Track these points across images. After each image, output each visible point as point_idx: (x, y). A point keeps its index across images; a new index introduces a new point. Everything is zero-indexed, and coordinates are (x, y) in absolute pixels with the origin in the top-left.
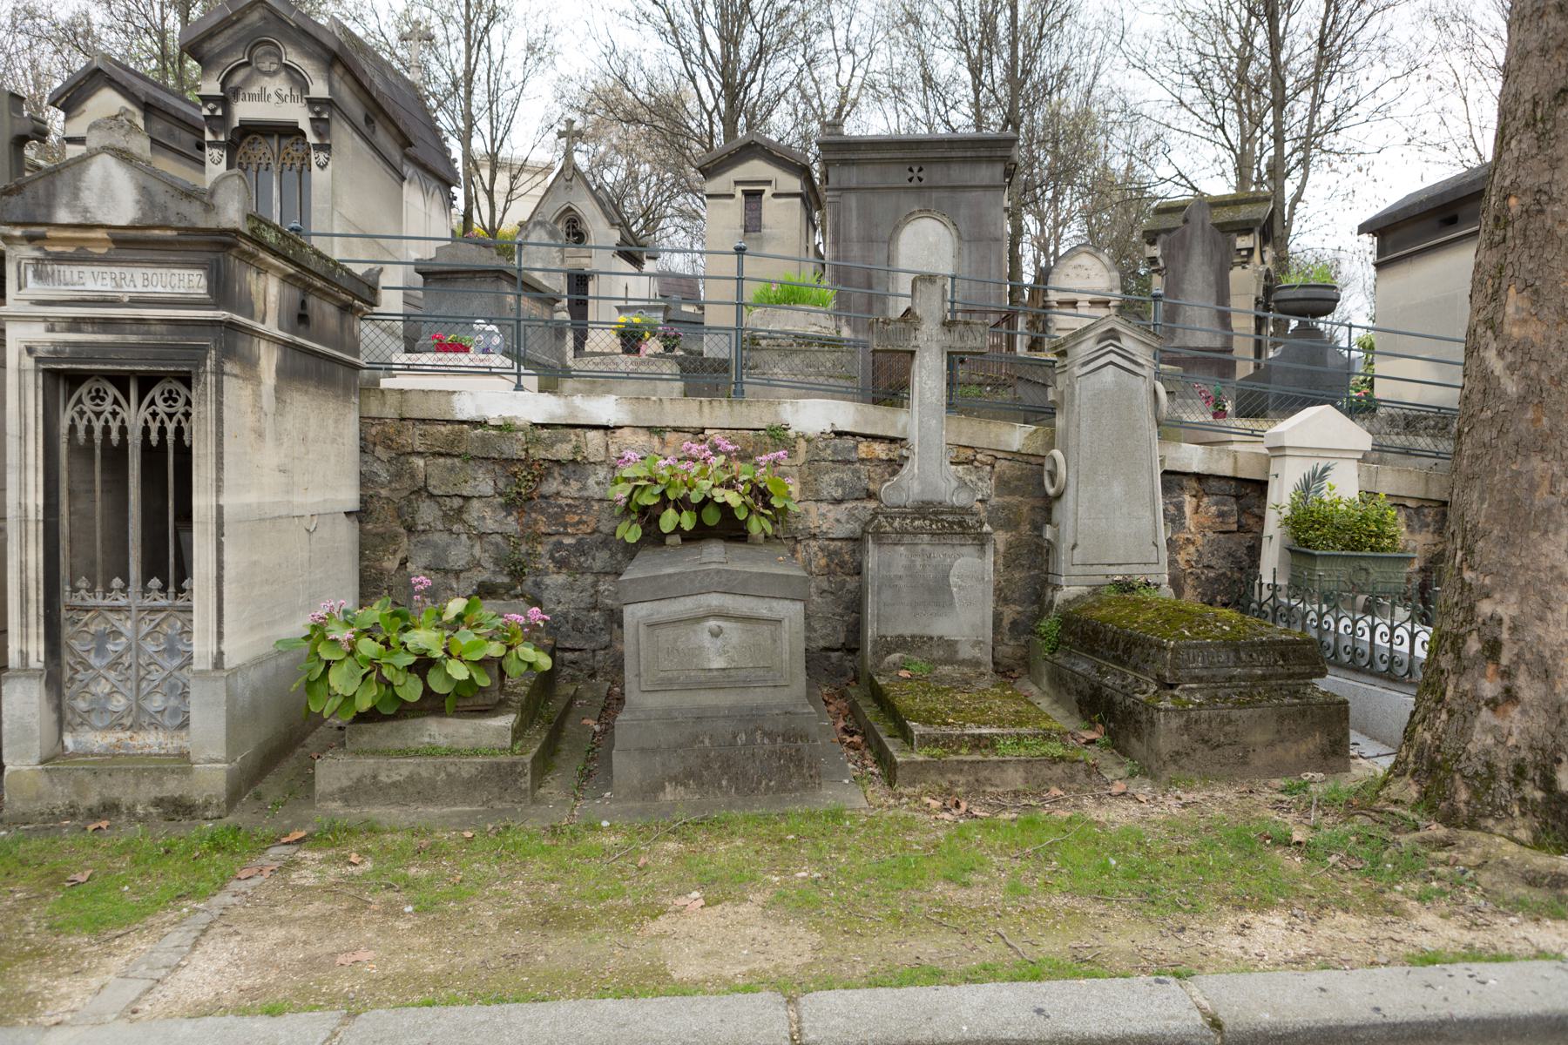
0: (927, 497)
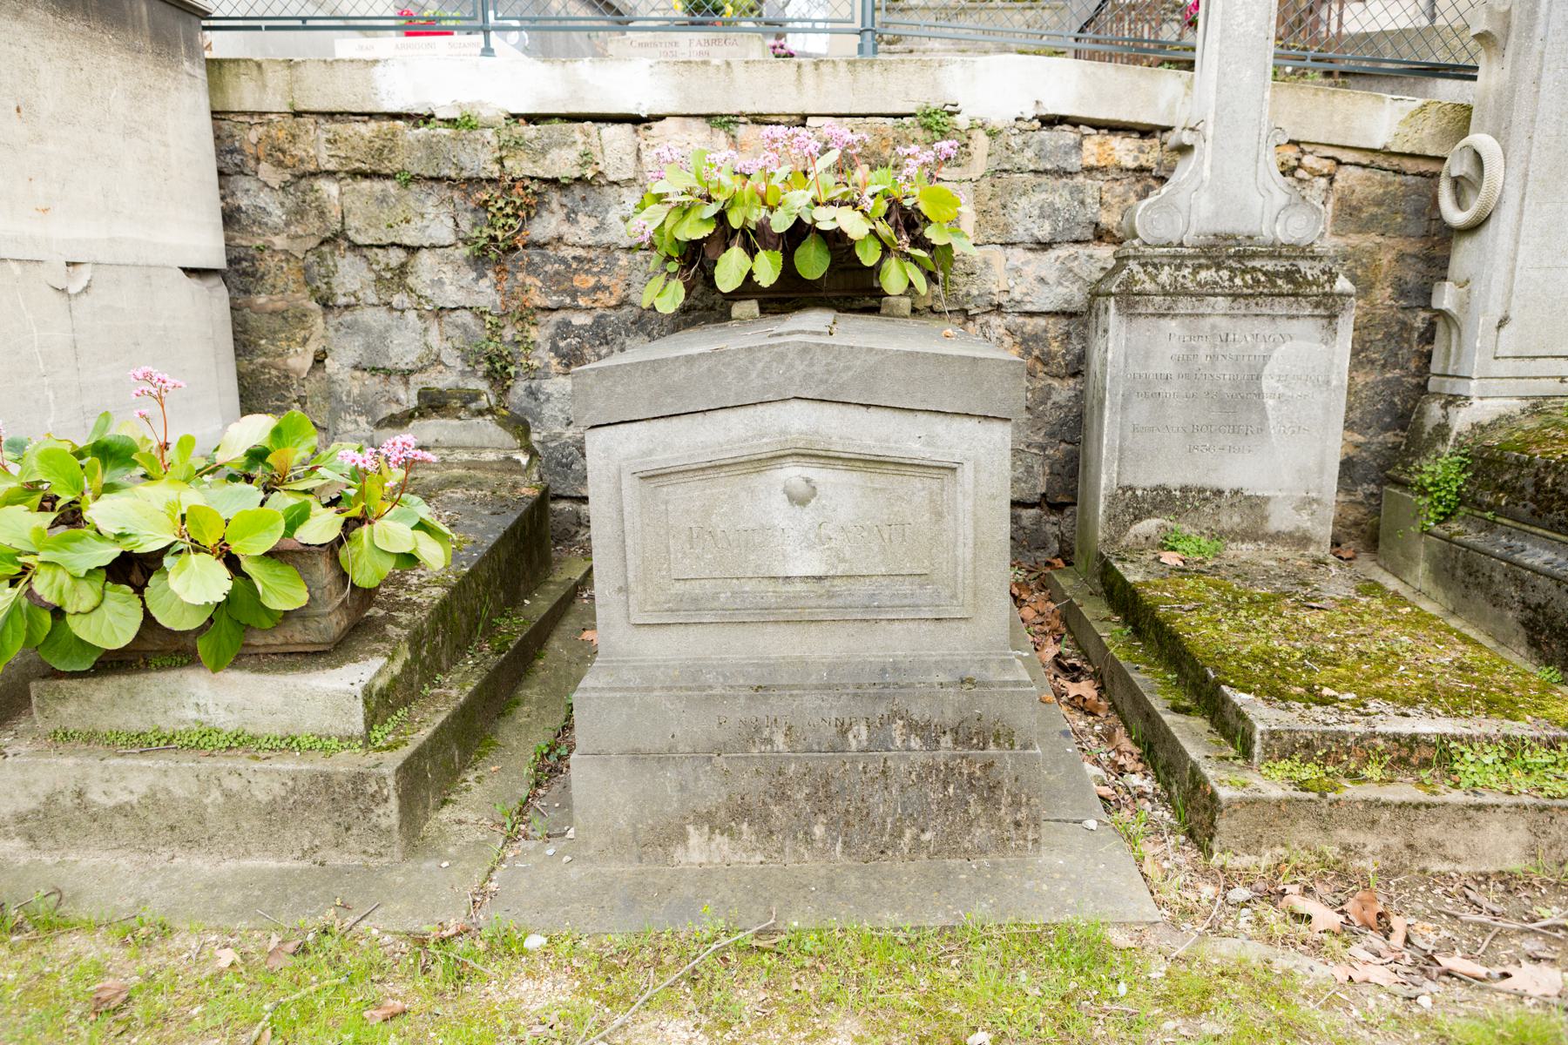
0: (1225, 226)
